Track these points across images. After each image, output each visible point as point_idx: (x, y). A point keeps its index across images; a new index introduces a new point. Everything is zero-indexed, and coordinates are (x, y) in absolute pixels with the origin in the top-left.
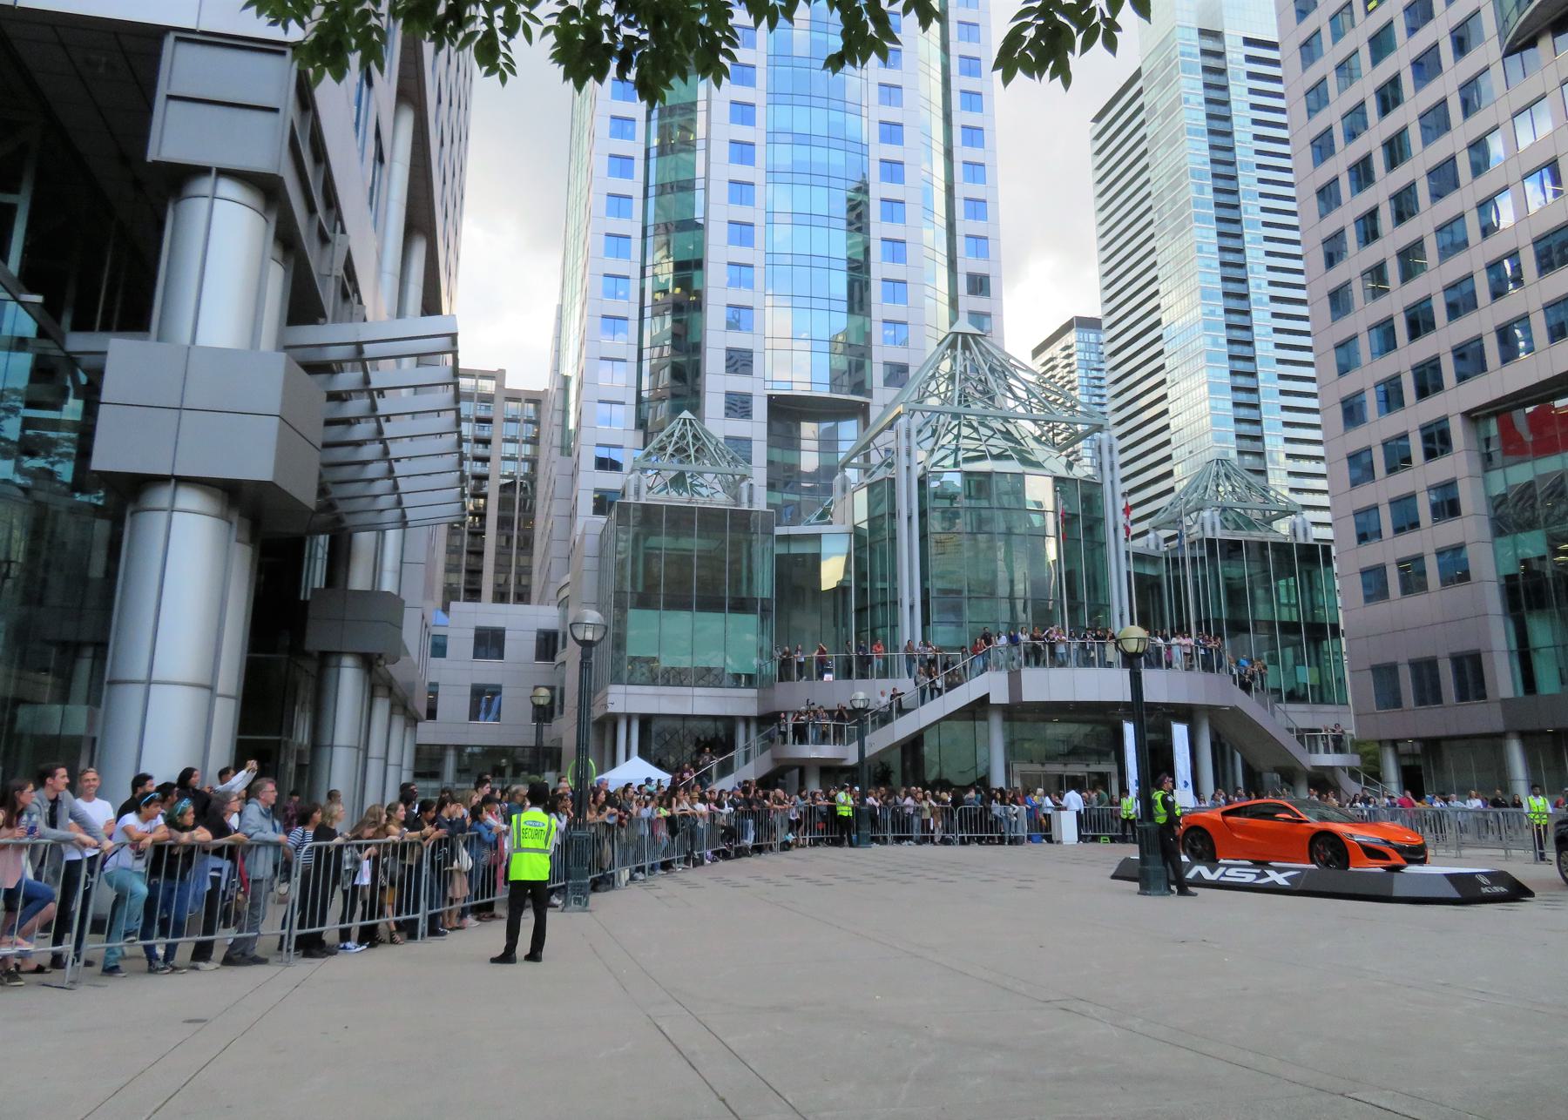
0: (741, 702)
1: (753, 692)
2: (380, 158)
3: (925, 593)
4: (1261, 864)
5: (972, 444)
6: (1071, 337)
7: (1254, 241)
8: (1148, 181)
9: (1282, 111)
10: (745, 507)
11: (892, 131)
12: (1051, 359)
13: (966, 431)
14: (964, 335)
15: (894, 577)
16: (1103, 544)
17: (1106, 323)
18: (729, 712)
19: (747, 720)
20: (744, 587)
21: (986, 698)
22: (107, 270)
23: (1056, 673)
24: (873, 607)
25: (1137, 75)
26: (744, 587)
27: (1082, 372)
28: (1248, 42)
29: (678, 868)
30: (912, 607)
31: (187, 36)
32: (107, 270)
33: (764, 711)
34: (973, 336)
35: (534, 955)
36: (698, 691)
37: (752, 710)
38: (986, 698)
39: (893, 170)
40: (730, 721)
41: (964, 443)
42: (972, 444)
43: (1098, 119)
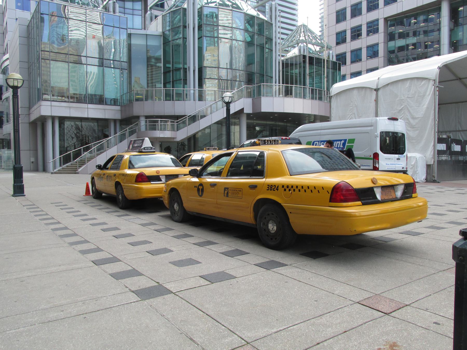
1: (118, 108)
18: (107, 117)
19: (115, 121)
33: (125, 117)
36: (90, 106)
37: (118, 116)
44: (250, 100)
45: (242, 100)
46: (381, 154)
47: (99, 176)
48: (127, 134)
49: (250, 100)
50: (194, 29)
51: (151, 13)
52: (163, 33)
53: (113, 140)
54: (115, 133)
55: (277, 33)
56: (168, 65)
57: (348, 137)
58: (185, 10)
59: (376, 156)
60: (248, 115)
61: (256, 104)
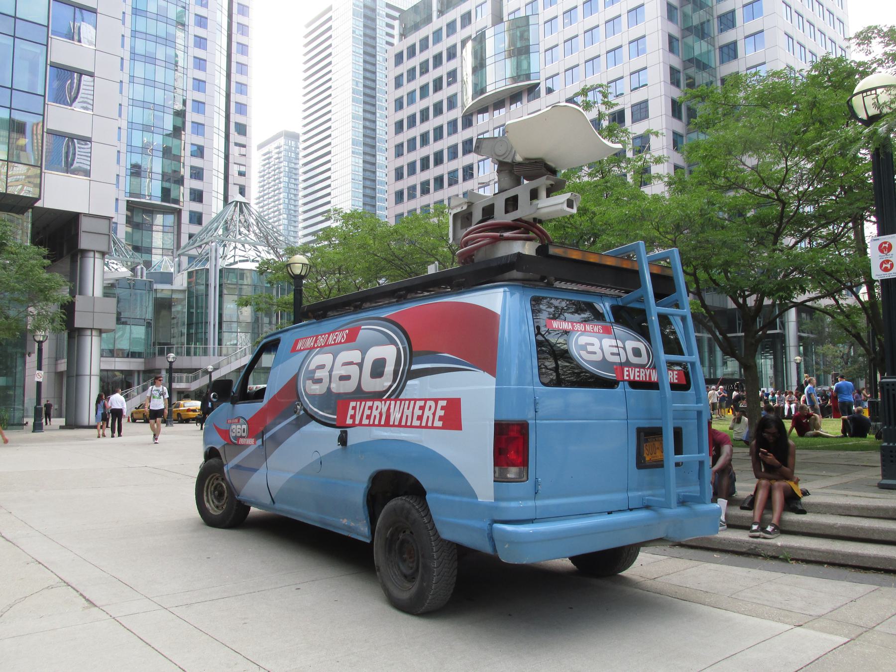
0: (134, 364)
1: (142, 360)
2: (610, 513)
3: (221, 316)
5: (243, 253)
6: (282, 141)
7: (381, 117)
8: (330, 71)
10: (764, 482)
11: (200, 85)
12: (269, 153)
14: (241, 203)
15: (207, 307)
17: (302, 138)
18: (132, 368)
19: (139, 372)
24: (197, 324)
25: (330, 9)
27: (285, 163)
28: (389, 6)
29: (286, 340)
31: (85, 215)
34: (245, 203)
35: (120, 435)
37: (142, 368)
39: (199, 106)
40: (128, 373)
42: (243, 253)
43: (308, 26)
47: (136, 413)
52: (190, 291)
54: (139, 384)
58: (208, 270)
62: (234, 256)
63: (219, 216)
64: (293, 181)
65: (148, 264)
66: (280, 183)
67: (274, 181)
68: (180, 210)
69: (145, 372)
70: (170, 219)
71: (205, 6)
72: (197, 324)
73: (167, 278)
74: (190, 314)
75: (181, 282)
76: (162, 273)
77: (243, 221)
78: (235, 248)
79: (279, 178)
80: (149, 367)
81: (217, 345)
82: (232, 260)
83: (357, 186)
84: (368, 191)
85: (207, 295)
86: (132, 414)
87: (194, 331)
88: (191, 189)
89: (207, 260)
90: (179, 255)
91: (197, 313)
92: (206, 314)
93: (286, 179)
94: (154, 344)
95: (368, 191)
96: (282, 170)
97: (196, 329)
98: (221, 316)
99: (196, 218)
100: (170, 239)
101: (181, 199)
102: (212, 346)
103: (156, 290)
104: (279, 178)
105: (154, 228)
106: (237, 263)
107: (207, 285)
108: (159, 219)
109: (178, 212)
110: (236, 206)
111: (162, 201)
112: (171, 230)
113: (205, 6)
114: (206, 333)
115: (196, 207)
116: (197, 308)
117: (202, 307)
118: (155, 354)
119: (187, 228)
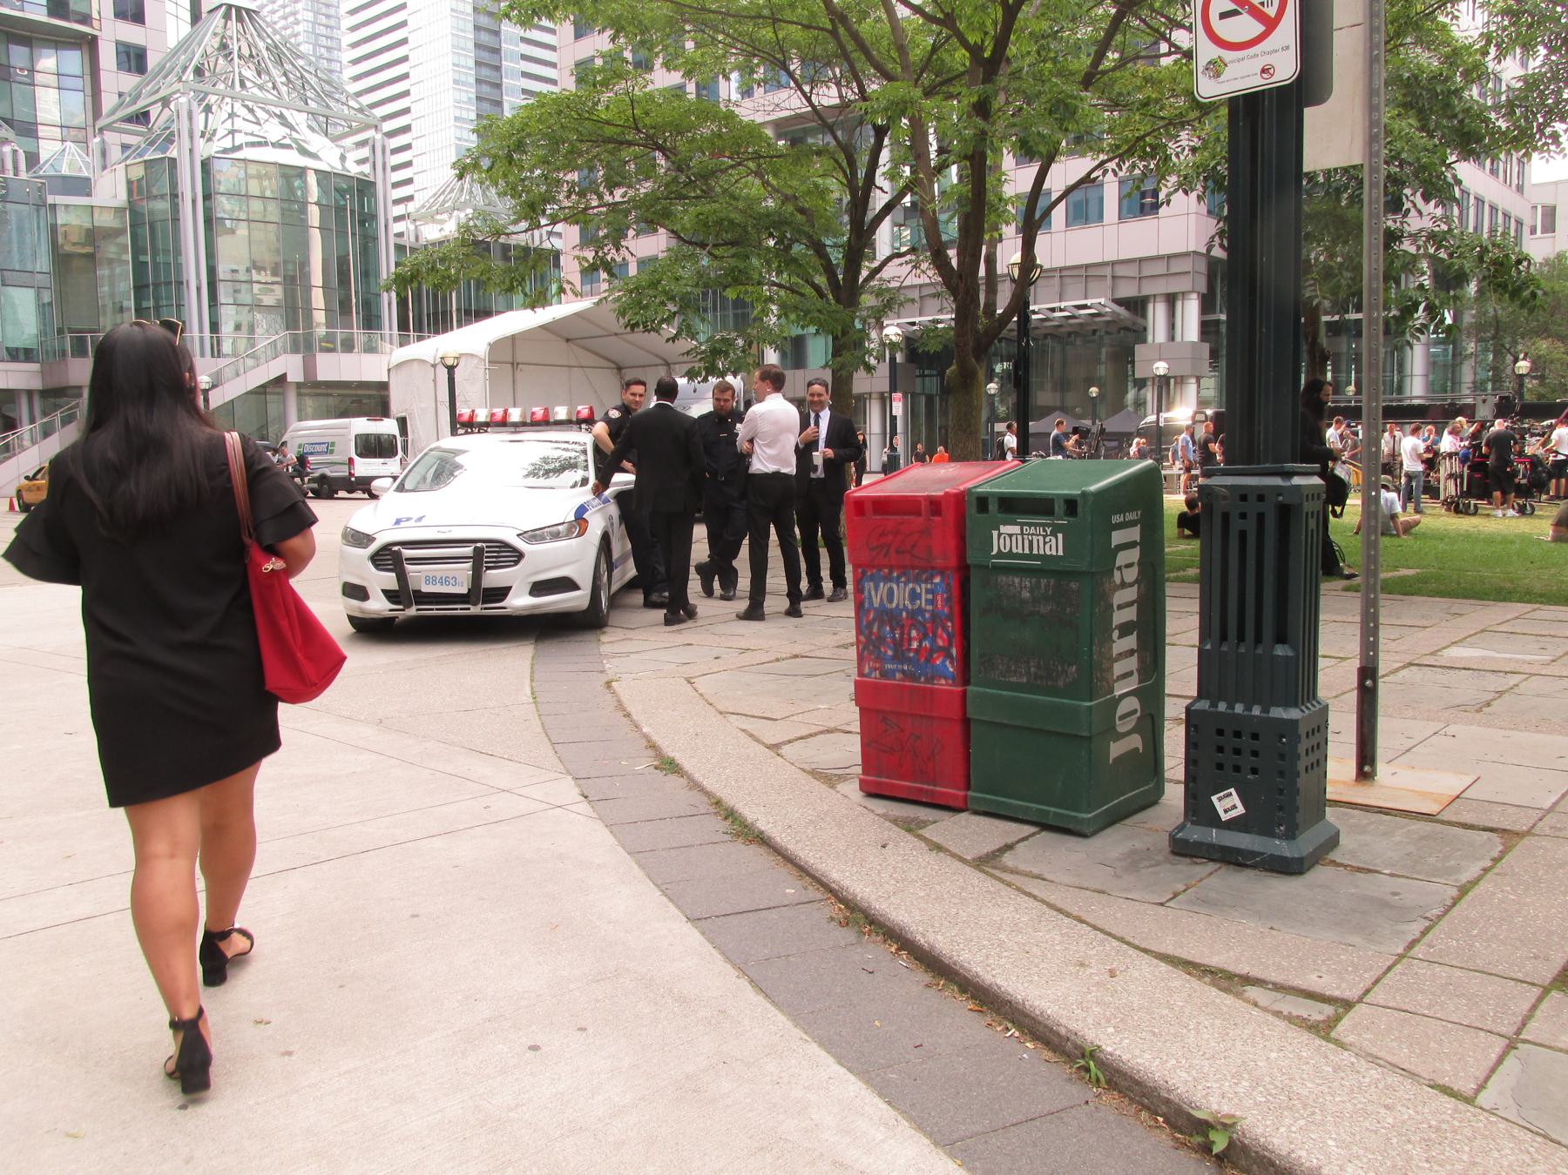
1: (35, 367)
3: (212, 271)
4: (1450, 185)
9: (553, 48)
13: (243, 112)
14: (239, 9)
15: (178, 252)
16: (375, 239)
18: (11, 386)
19: (30, 393)
20: (16, 257)
21: (284, 376)
22: (802, 558)
23: (345, 358)
24: (157, 285)
26: (16, 257)
30: (199, 289)
32: (802, 558)
33: (50, 386)
34: (248, 11)
37: (37, 384)
38: (284, 376)
41: (239, 124)
44: (298, 359)
45: (282, 358)
46: (357, 459)
47: (29, 489)
48: (58, 422)
49: (298, 359)
50: (194, 202)
51: (103, 141)
52: (133, 208)
53: (27, 436)
54: (32, 421)
55: (386, 195)
56: (142, 258)
57: (330, 440)
58: (173, 161)
59: (351, 461)
60: (299, 385)
61: (309, 366)
62: (232, 132)
63: (184, 45)
64: (323, 20)
65: (33, 159)
66: (297, 23)
67: (285, 18)
68: (95, 39)
69: (45, 393)
70: (73, 60)
71: (138, 17)
72: (157, 285)
73: (81, 186)
74: (139, 267)
75: (111, 191)
76: (64, 177)
77: (246, 52)
78: (232, 115)
79: (294, 14)
80: (54, 383)
81: (207, 333)
82: (227, 143)
83: (461, 24)
84: (485, 38)
85: (176, 220)
86: (19, 491)
87: (151, 303)
88: (118, 43)
89: (170, 140)
90: (101, 130)
91: (156, 264)
92: (179, 267)
93: (310, 16)
94: (60, 331)
95: (485, 38)
96: (299, 17)
97: (157, 299)
98: (212, 271)
99: (134, 59)
100: (77, 103)
101: (95, 15)
102: (196, 334)
103: (54, 207)
104: (294, 14)
105: (39, 78)
106: (240, 148)
107: (174, 196)
108: (48, 61)
109: (90, 44)
110: (227, 17)
111: (51, 14)
112: (79, 83)
113: (138, 17)
114: (179, 306)
115: (130, 33)
116: (155, 253)
117: (166, 252)
118: (64, 353)
119: (115, 81)
